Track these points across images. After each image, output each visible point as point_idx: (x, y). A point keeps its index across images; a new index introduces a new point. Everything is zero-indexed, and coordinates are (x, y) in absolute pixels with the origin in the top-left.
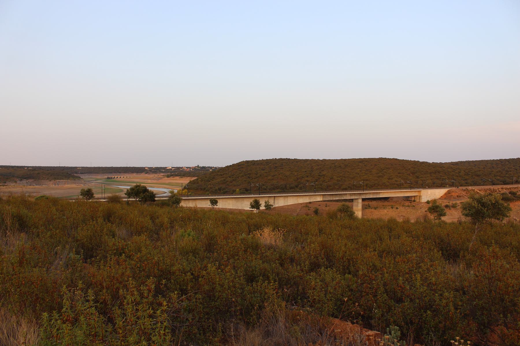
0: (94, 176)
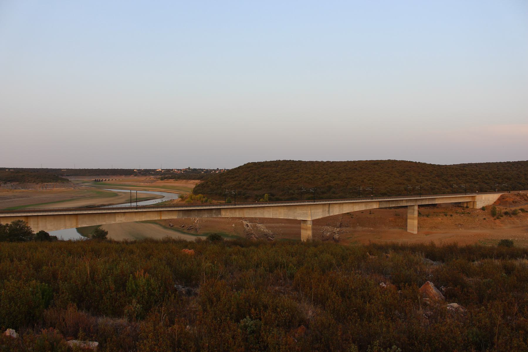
0: (81, 179)
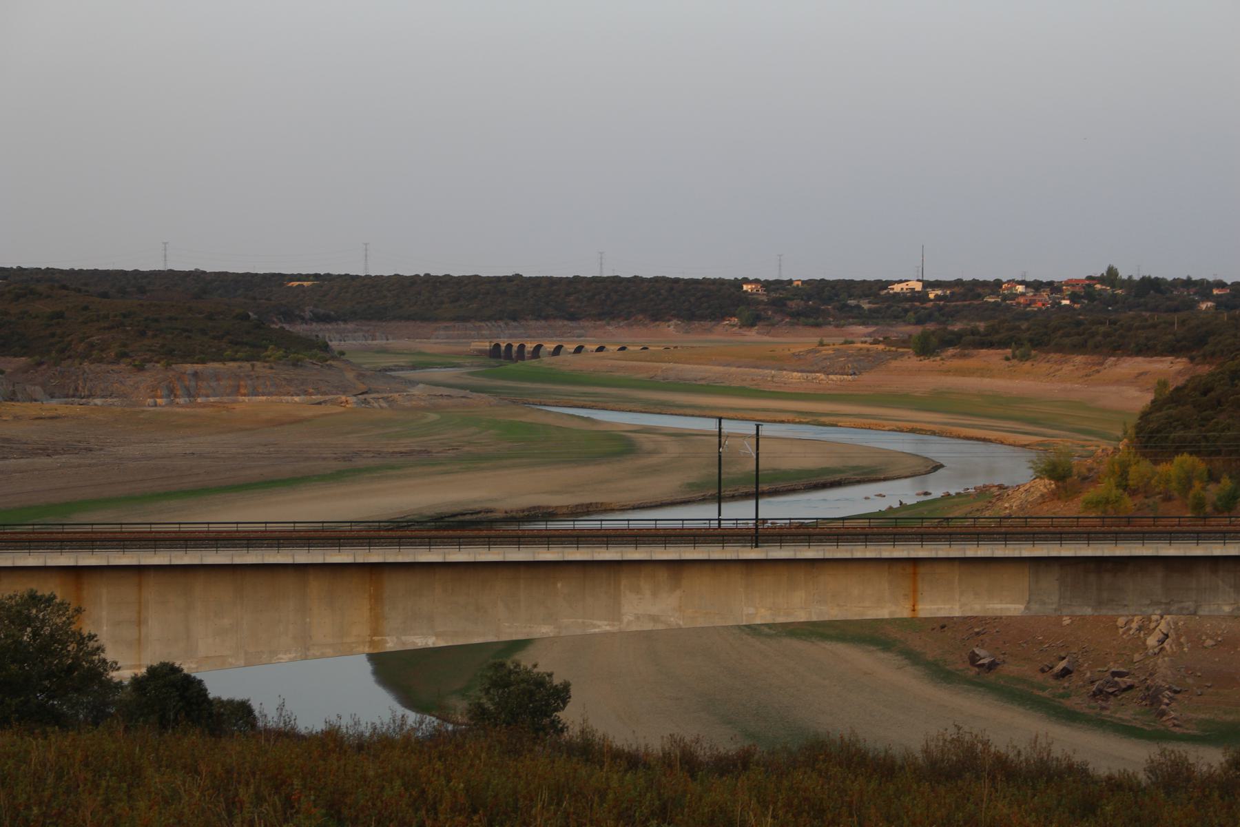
0: (405, 342)
